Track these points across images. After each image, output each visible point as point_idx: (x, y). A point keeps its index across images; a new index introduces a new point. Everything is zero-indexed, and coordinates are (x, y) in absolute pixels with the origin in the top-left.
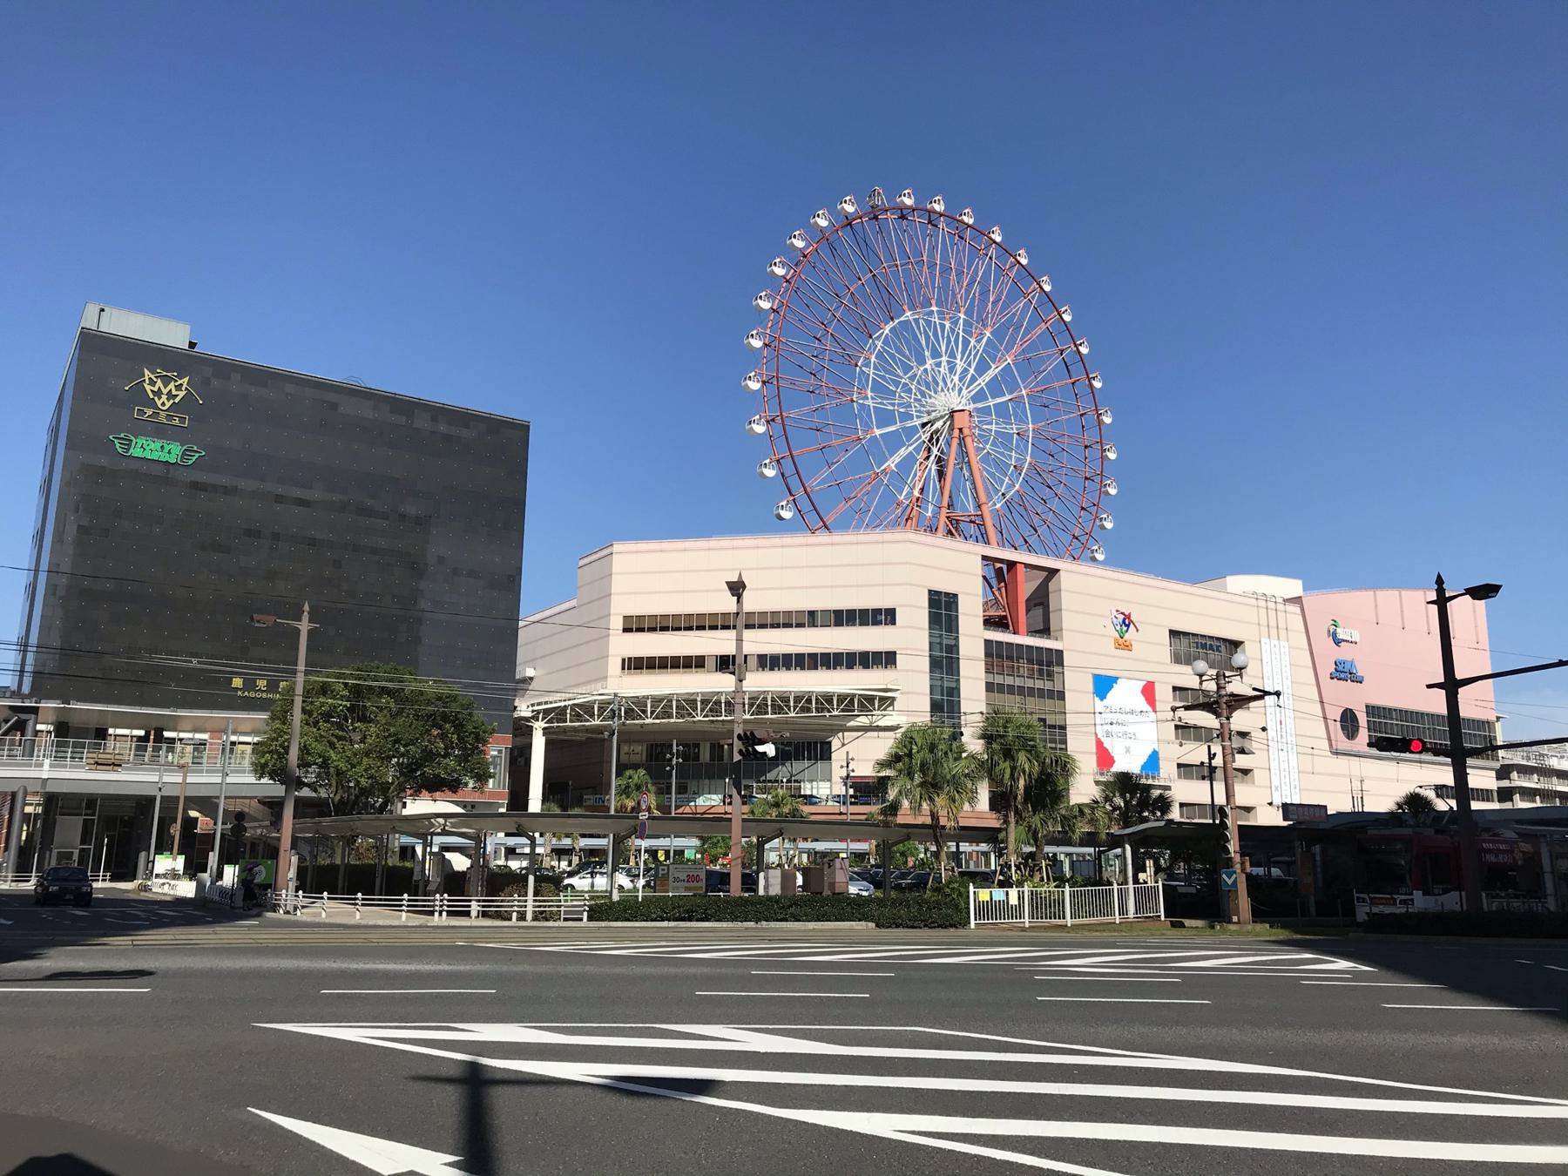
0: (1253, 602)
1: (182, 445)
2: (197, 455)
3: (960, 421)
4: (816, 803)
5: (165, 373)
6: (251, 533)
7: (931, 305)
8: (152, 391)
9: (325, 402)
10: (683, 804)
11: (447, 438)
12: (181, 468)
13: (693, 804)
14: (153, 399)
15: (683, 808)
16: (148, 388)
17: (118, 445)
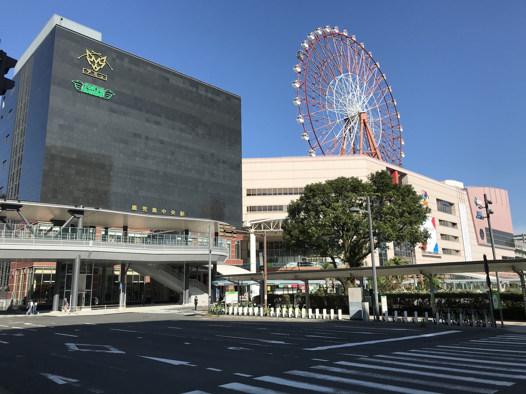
0: (455, 189)
1: (105, 89)
2: (112, 95)
3: (363, 116)
4: (312, 266)
5: (96, 53)
6: (137, 135)
7: (348, 72)
8: (90, 61)
9: (164, 77)
10: (281, 266)
11: (212, 100)
12: (104, 101)
13: (285, 266)
14: (91, 65)
15: (281, 268)
16: (89, 59)
17: (76, 86)
